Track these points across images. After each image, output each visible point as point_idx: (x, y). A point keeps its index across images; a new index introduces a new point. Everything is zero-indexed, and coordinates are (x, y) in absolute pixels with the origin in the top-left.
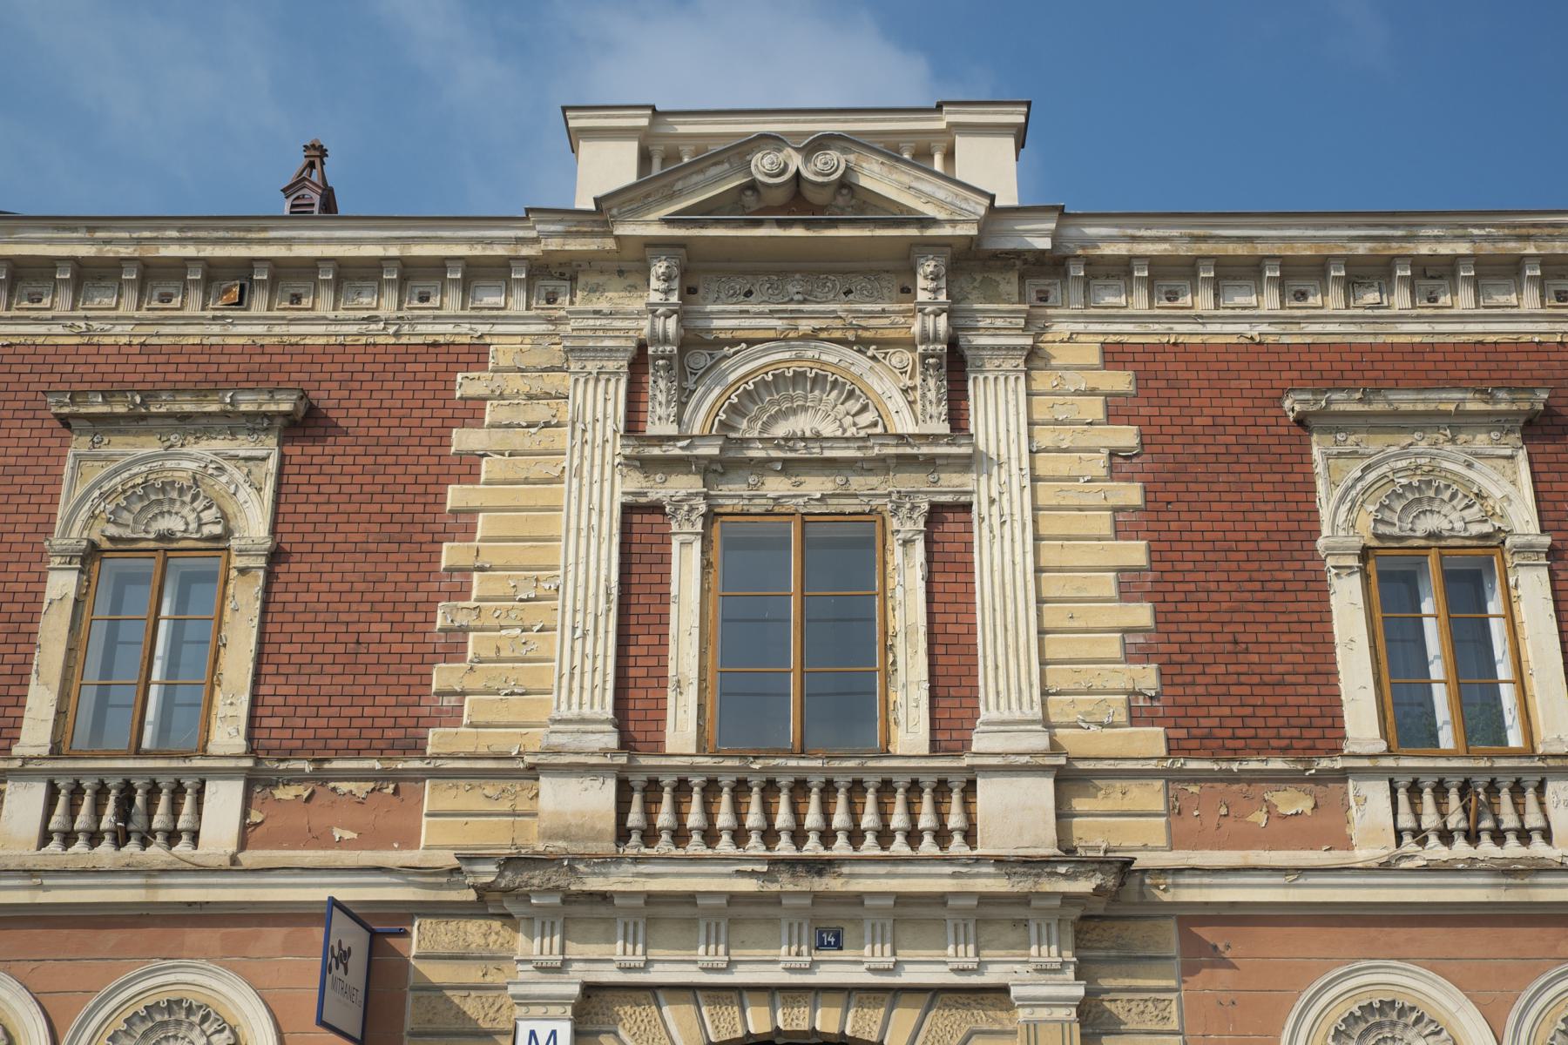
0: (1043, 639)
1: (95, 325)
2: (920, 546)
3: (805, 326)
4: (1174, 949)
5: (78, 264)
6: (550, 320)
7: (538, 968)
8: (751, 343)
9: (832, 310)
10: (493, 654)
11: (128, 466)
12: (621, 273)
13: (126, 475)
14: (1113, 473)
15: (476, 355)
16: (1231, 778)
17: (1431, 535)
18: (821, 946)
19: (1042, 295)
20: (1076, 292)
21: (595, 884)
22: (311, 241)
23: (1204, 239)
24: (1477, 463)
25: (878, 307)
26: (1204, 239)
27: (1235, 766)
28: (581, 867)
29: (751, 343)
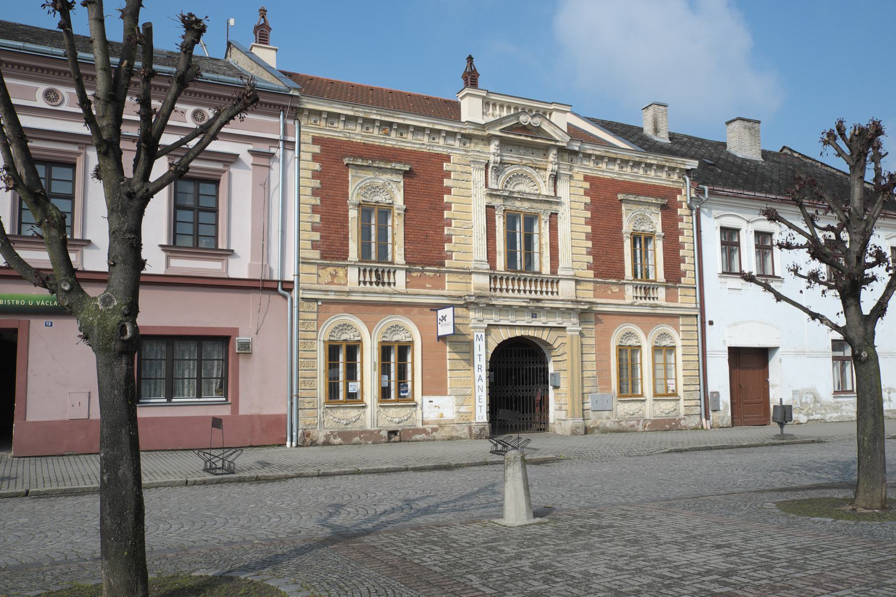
0: (134, 141)
1: (352, 135)
2: (548, 223)
3: (524, 162)
4: (594, 320)
5: (347, 116)
6: (465, 151)
7: (478, 321)
8: (512, 164)
9: (529, 158)
11: (365, 180)
12: (482, 140)
13: (365, 183)
15: (447, 158)
16: (605, 283)
17: (643, 231)
18: (533, 317)
19: (263, 12)
20: (579, 160)
21: (494, 302)
22: (410, 120)
23: (608, 152)
24: (652, 214)
25: (540, 159)
26: (608, 152)
27: (607, 281)
28: (492, 299)
29: (512, 164)
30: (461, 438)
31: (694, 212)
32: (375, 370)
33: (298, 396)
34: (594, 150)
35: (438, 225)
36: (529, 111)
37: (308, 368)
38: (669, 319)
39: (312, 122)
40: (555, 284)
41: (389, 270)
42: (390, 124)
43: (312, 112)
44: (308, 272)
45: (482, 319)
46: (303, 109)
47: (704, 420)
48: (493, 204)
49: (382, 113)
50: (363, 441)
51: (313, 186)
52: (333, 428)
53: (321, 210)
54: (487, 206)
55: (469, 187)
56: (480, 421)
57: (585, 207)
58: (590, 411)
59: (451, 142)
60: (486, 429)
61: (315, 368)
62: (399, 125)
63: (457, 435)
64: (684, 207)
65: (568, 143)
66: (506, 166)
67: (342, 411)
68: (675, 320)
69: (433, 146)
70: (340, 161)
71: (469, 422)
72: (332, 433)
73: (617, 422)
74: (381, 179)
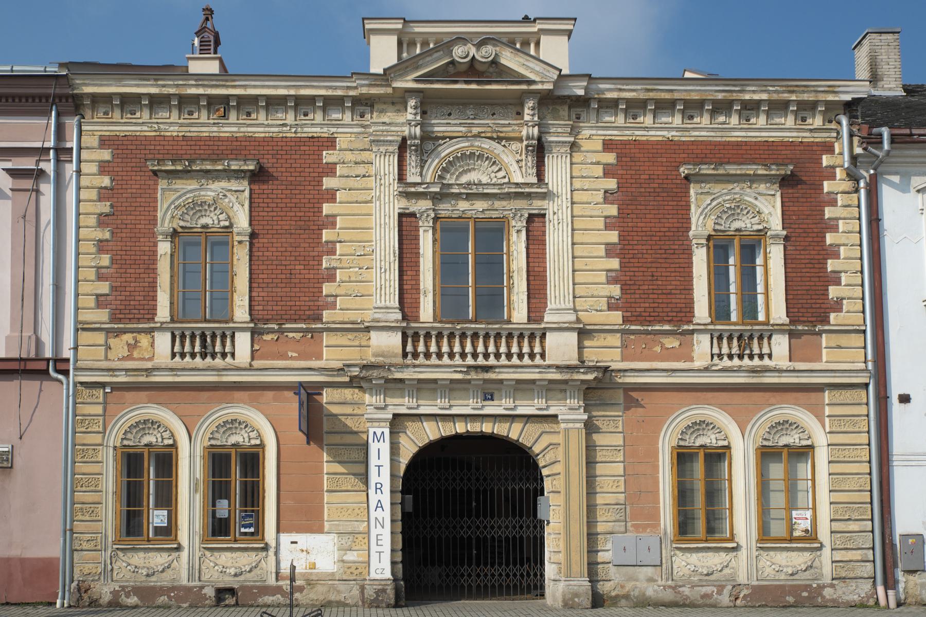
1: (162, 126)
2: (524, 233)
3: (475, 130)
4: (622, 401)
5: (151, 96)
8: (451, 138)
9: (485, 123)
12: (393, 103)
13: (184, 198)
14: (606, 200)
15: (331, 143)
16: (647, 333)
17: (738, 230)
18: (485, 399)
20: (593, 115)
21: (398, 375)
22: (255, 87)
23: (652, 90)
24: (760, 198)
25: (507, 122)
26: (652, 90)
27: (650, 328)
28: (392, 369)
29: (451, 138)
30: (345, 605)
31: (862, 184)
32: (196, 491)
33: (71, 530)
34: (620, 90)
35: (311, 254)
37: (88, 489)
38: (799, 395)
39: (101, 115)
40: (766, 341)
41: (751, 335)
42: (226, 99)
43: (97, 100)
44: (91, 343)
45: (382, 404)
46: (82, 96)
47: (880, 590)
48: (412, 210)
49: (206, 83)
50: (173, 602)
51: (99, 212)
52: (127, 581)
53: (114, 248)
54: (401, 215)
55: (369, 186)
57: (605, 198)
58: (610, 565)
60: (388, 591)
61: (99, 488)
62: (239, 98)
63: (338, 599)
64: (838, 176)
65: (556, 83)
66: (441, 142)
67: (141, 554)
68: (813, 395)
69: (303, 126)
70: (143, 169)
71: (362, 578)
72: (123, 588)
73: (670, 587)
74: (210, 190)
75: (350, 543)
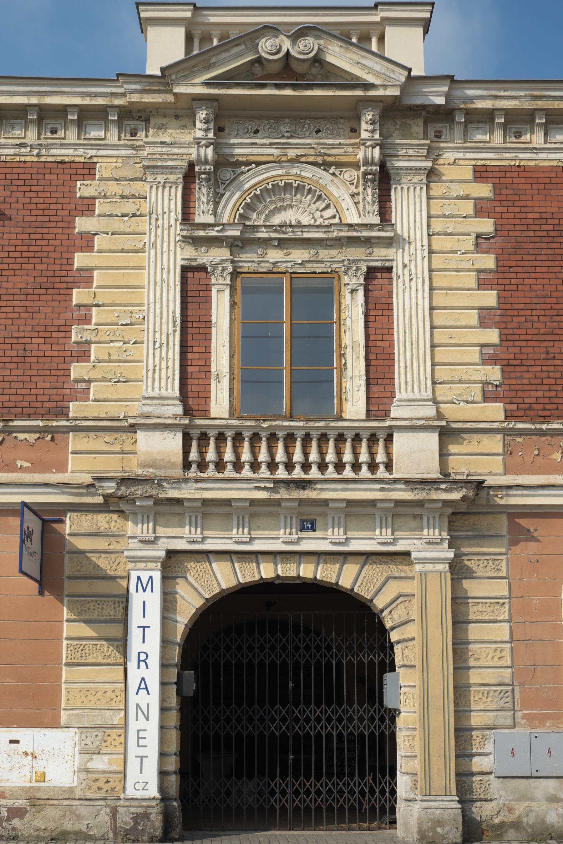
3: (292, 153)
4: (505, 531)
6: (134, 148)
8: (258, 164)
10: (106, 358)
12: (177, 117)
14: (478, 248)
16: (541, 433)
18: (303, 529)
20: (459, 132)
21: (173, 494)
25: (336, 142)
27: (544, 427)
28: (165, 484)
29: (258, 164)
34: (496, 97)
35: (56, 322)
36: (359, 39)
56: (139, 794)
58: (492, 777)
59: (96, 133)
60: (152, 817)
63: (76, 828)
65: (404, 88)
75: (98, 743)
